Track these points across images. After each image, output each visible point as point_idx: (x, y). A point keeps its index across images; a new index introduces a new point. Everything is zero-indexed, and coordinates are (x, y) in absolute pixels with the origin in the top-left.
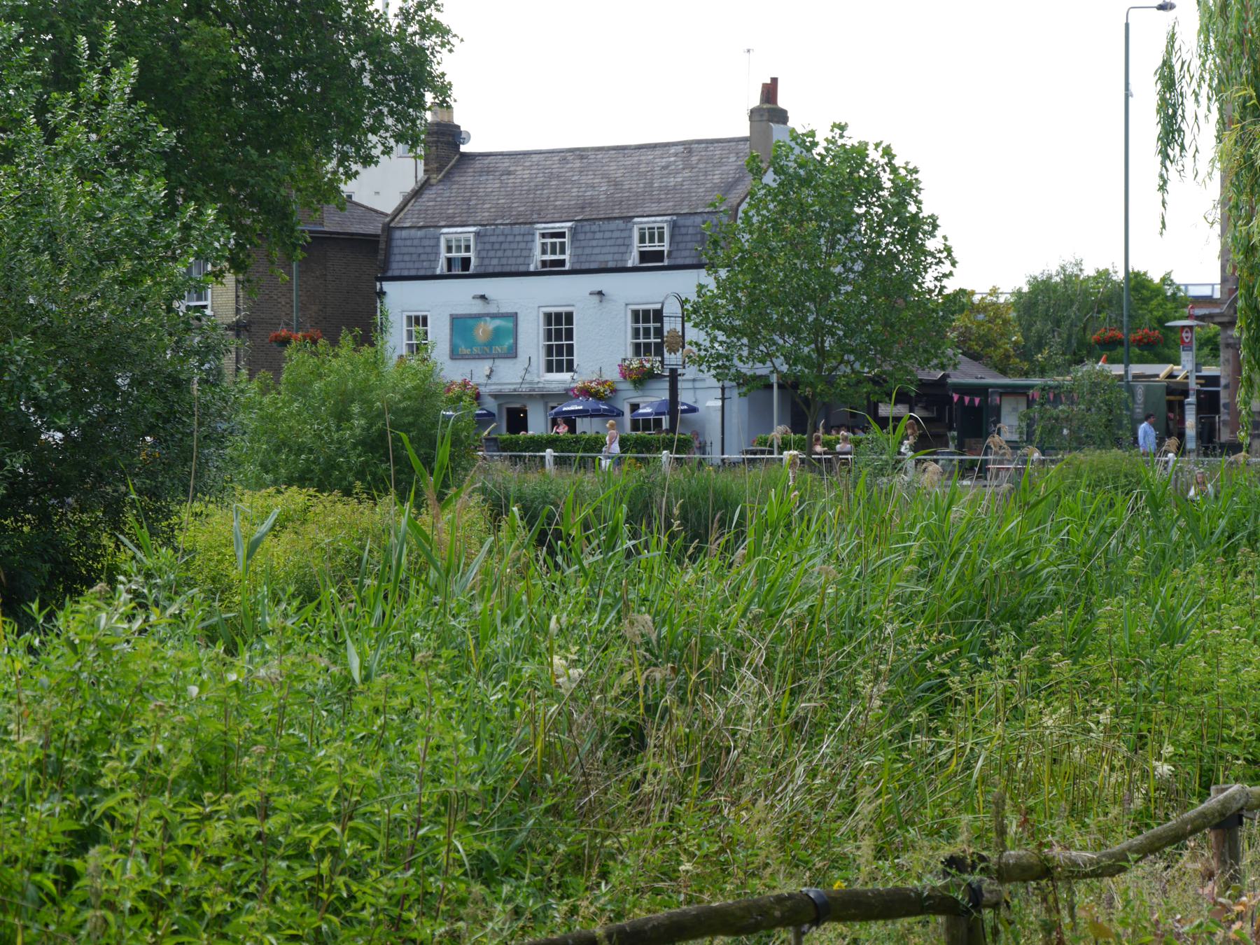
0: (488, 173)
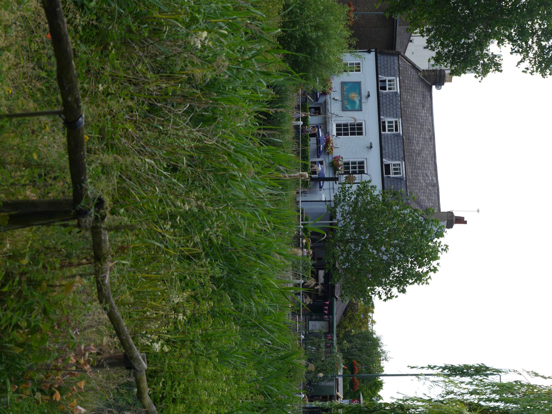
0: (423, 98)
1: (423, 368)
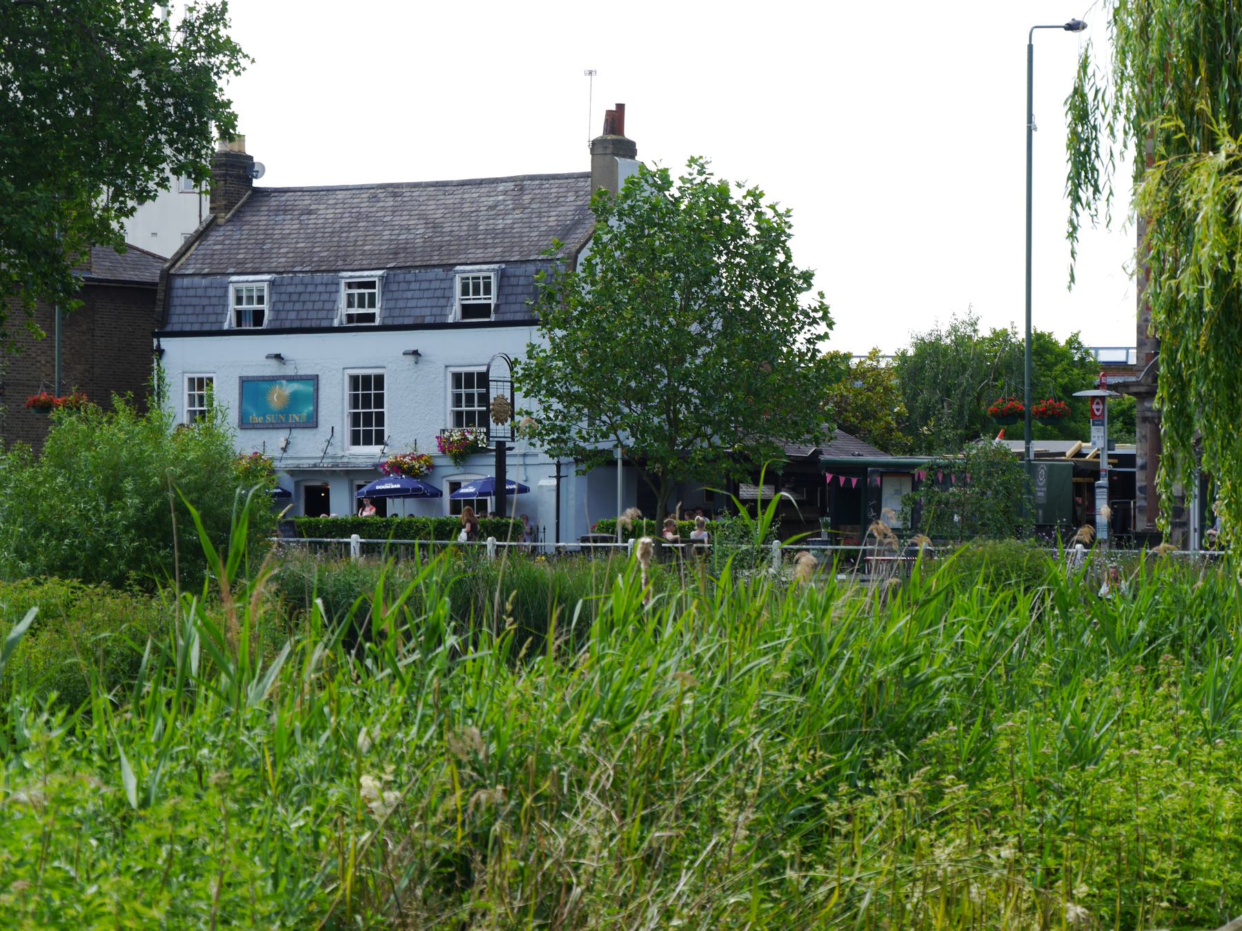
1: (1073, 253)
